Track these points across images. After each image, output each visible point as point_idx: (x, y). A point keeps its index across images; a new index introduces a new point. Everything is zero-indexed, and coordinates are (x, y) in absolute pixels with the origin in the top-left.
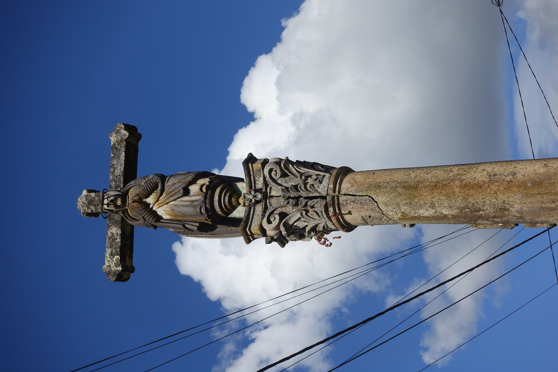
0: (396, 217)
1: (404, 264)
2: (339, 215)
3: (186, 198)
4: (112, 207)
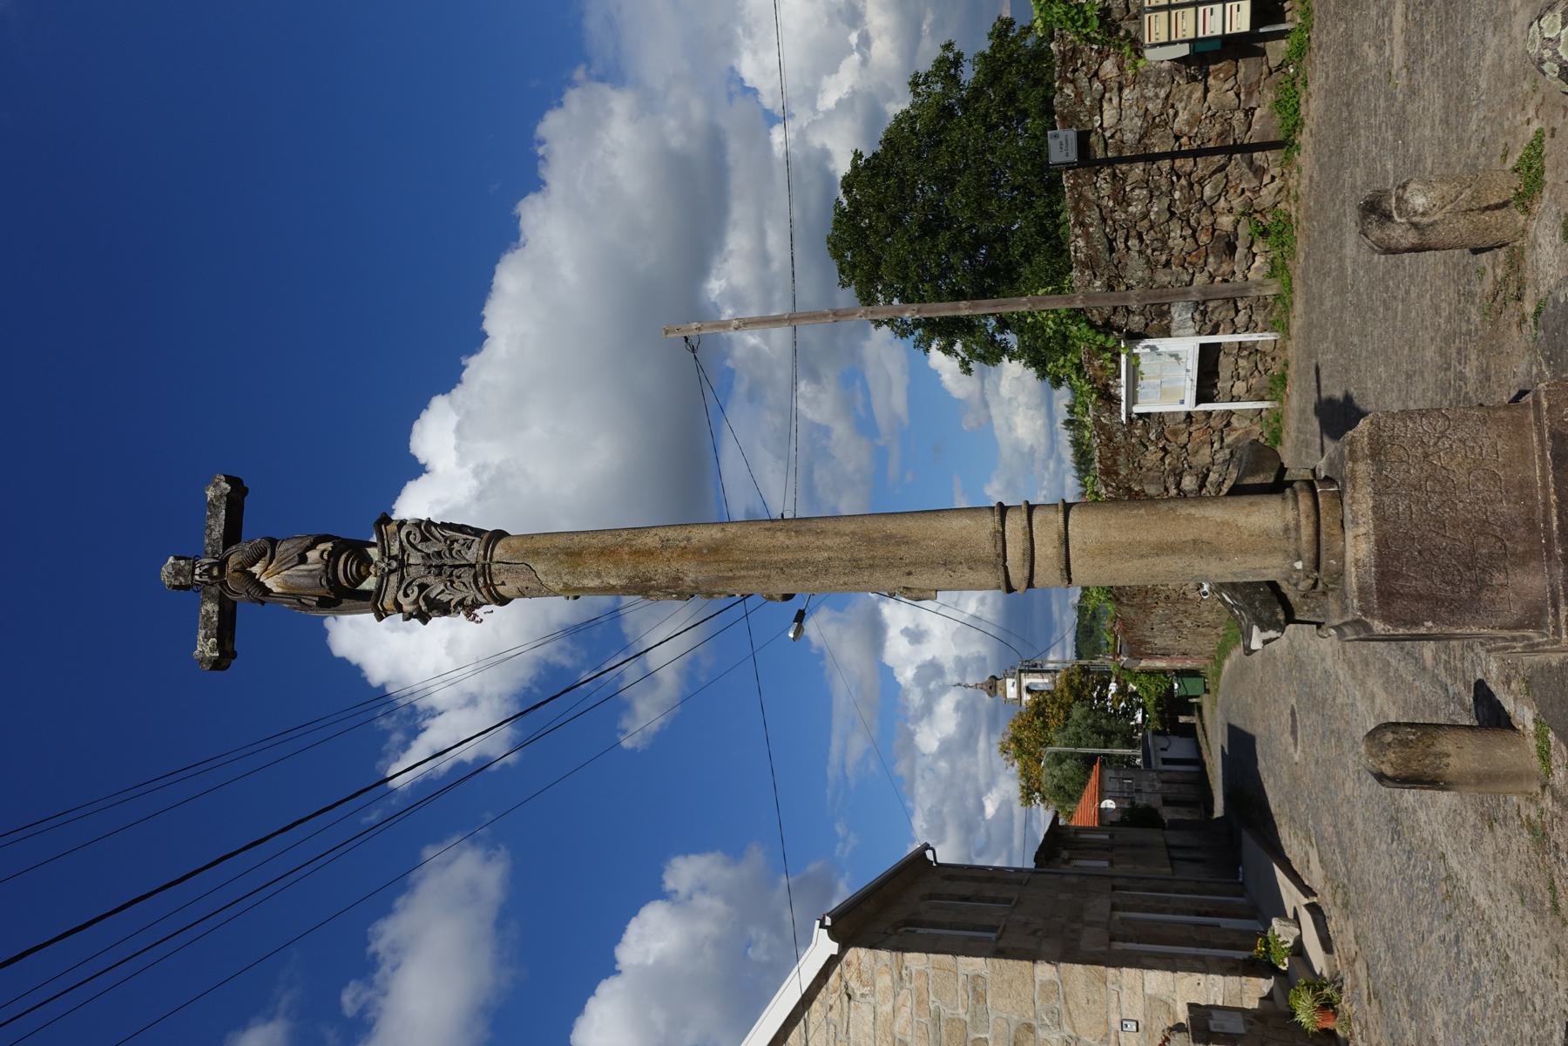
0: (557, 588)
1: (599, 639)
2: (490, 586)
3: (302, 567)
4: (205, 578)
